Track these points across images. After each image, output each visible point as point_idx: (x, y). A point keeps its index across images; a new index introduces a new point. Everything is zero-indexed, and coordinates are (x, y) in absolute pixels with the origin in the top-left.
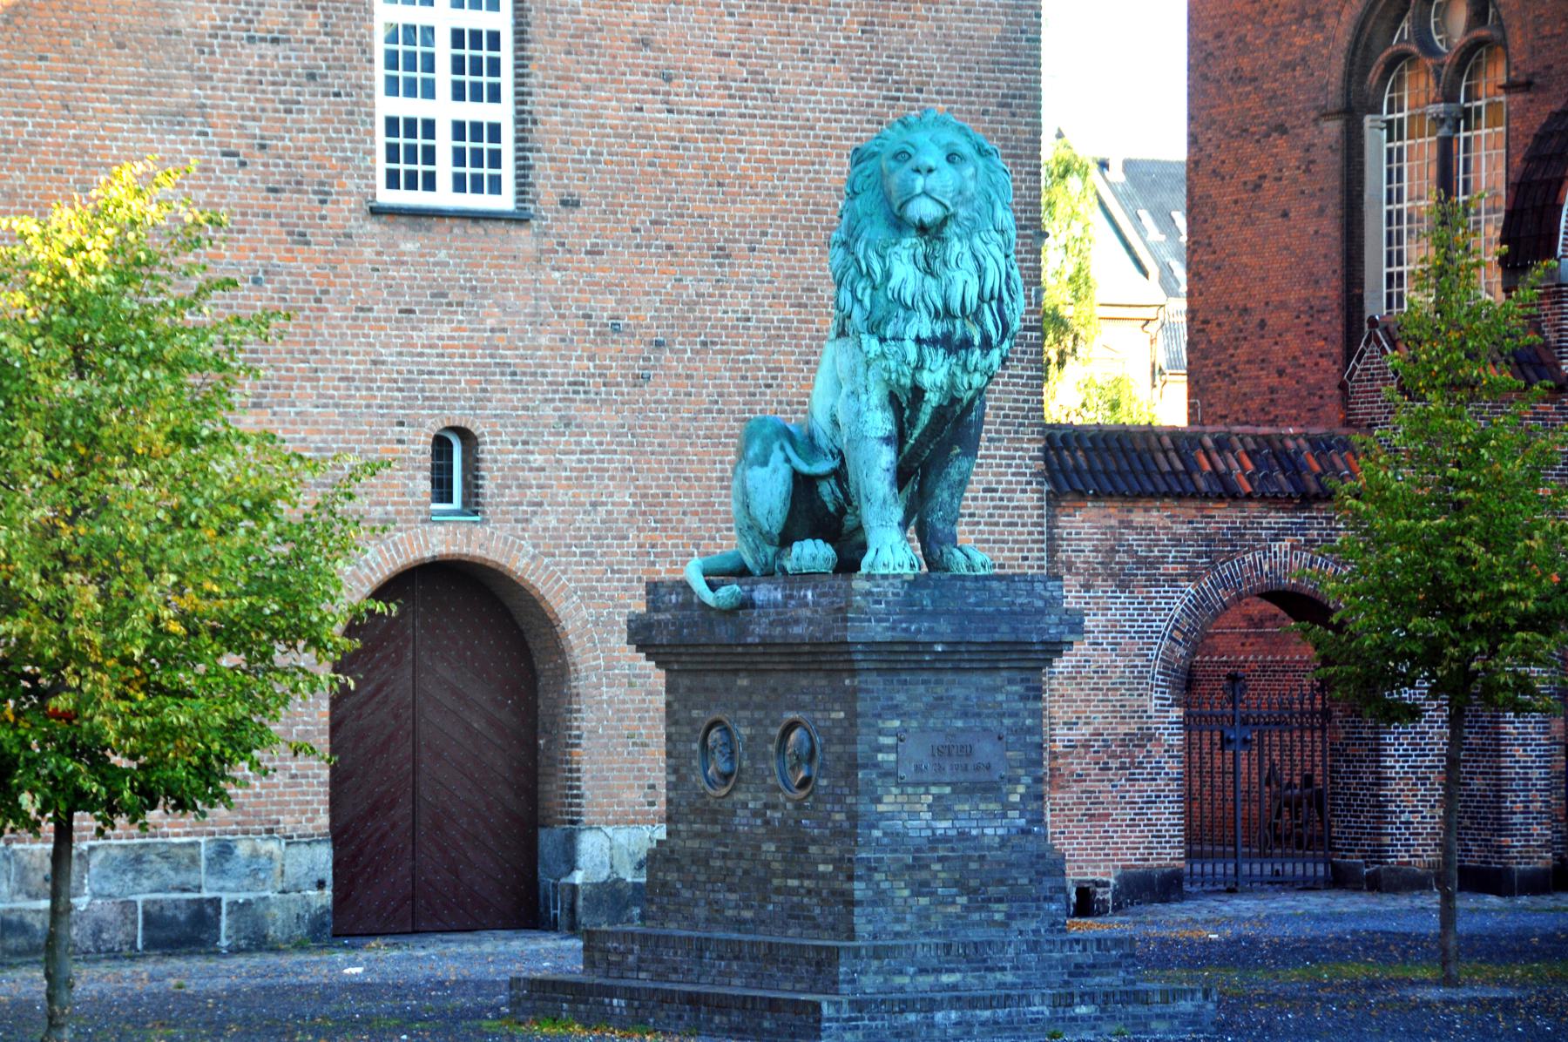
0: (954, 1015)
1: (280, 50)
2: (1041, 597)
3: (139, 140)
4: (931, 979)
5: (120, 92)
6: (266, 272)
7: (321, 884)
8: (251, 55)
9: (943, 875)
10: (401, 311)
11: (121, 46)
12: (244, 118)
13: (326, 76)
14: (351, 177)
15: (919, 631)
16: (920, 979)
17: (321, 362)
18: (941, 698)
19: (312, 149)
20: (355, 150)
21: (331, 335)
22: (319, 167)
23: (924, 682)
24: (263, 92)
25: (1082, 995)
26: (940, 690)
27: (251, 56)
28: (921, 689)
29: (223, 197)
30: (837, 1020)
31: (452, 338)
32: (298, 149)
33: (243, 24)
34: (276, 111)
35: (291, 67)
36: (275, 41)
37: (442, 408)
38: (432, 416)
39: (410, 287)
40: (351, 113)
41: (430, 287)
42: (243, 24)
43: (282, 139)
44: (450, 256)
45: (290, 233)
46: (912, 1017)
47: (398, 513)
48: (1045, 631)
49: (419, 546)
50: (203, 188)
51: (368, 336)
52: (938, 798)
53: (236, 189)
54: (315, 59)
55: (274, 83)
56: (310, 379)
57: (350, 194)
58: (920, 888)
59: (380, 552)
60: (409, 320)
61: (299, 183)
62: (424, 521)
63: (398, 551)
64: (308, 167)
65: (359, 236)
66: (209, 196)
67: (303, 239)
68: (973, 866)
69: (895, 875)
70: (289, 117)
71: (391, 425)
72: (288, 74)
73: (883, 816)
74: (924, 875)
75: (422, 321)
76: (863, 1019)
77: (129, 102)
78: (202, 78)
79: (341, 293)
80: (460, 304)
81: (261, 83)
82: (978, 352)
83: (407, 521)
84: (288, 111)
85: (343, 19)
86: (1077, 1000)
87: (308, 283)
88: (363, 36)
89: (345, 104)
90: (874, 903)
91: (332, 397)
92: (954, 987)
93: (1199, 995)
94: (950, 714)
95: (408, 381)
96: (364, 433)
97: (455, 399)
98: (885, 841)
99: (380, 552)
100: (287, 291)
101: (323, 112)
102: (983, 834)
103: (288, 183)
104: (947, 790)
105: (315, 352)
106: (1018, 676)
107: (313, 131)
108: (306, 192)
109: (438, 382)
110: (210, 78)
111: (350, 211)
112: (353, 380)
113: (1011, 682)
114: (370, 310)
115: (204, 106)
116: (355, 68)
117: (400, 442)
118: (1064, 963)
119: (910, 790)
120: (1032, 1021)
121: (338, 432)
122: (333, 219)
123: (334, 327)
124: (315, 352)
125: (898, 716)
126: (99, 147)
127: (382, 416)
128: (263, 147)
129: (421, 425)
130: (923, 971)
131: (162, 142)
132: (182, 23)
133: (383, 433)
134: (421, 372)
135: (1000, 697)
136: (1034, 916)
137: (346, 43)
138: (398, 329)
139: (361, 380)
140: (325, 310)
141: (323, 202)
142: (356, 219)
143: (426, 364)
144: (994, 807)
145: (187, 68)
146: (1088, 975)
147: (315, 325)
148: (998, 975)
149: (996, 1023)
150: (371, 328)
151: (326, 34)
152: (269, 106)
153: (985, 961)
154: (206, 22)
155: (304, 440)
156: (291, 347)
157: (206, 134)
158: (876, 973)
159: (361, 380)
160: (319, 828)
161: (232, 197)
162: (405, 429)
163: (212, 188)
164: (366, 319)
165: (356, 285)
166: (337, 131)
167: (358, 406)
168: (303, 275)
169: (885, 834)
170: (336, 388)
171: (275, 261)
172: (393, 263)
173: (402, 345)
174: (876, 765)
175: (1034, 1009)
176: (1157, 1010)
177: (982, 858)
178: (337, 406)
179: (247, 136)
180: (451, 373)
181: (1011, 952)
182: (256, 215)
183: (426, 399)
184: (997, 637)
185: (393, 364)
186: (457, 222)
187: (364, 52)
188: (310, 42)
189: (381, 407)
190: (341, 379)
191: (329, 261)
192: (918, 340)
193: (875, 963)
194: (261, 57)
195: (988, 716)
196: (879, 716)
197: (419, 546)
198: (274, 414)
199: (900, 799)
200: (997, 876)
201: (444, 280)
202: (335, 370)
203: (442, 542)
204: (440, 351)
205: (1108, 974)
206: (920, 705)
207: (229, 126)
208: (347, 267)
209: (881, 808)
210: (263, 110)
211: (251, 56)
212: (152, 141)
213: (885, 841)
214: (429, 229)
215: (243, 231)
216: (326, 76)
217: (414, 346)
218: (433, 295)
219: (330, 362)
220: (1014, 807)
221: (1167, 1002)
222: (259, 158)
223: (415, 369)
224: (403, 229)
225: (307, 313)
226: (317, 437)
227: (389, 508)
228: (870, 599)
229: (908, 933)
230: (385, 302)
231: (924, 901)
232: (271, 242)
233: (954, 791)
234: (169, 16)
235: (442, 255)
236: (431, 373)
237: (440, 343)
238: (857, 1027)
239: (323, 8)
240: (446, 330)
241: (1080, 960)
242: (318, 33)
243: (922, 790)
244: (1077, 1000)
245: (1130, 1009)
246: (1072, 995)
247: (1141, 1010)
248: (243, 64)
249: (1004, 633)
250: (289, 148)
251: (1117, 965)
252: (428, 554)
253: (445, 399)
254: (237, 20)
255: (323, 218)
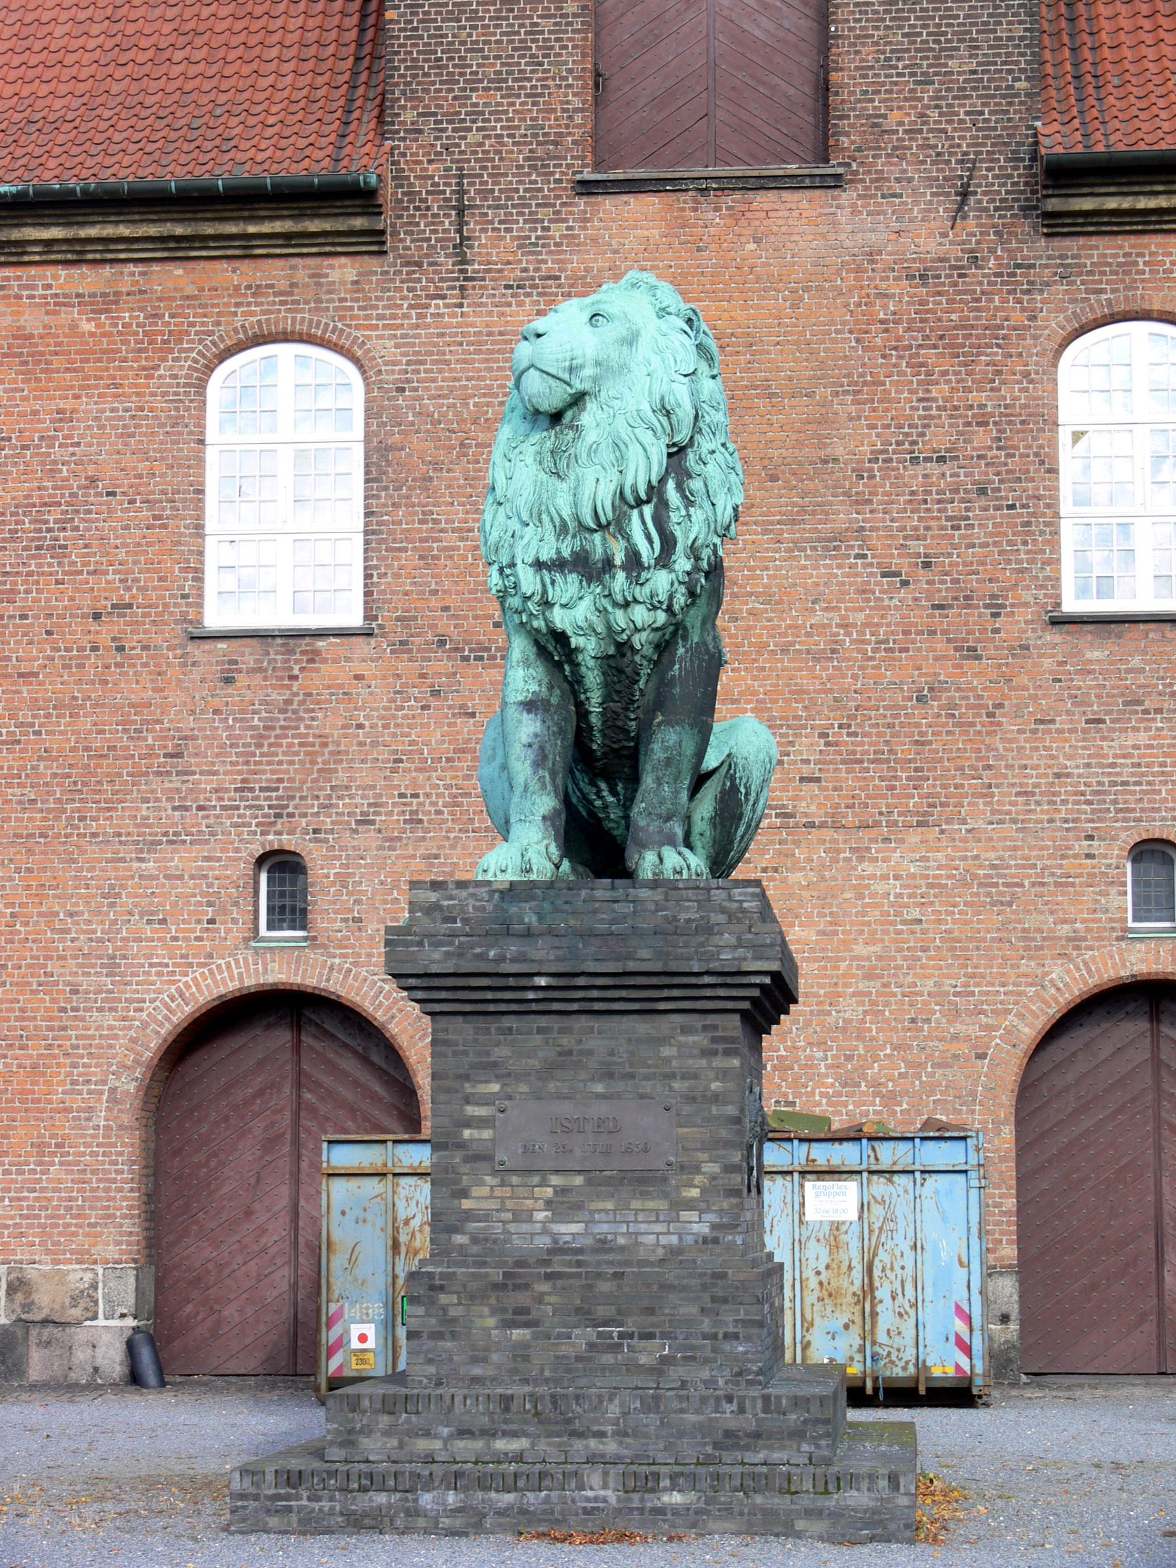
0: (451, 1498)
1: (947, 468)
2: (723, 910)
3: (791, 568)
4: (479, 1444)
5: (772, 523)
6: (931, 689)
7: (1005, 1319)
8: (914, 477)
9: (553, 1299)
10: (1088, 722)
11: (774, 478)
12: (905, 538)
13: (999, 490)
14: (1028, 588)
15: (501, 959)
16: (461, 1444)
17: (996, 776)
18: (570, 1053)
19: (983, 564)
20: (1031, 561)
21: (1005, 749)
22: (990, 580)
23: (540, 1031)
24: (928, 510)
25: (673, 1477)
26: (566, 1041)
27: (915, 476)
28: (538, 1039)
29: (882, 617)
30: (256, 1498)
31: (1151, 746)
32: (965, 564)
33: (907, 446)
34: (942, 528)
35: (958, 484)
36: (941, 459)
37: (1140, 820)
38: (1127, 829)
39: (1098, 696)
40: (1028, 524)
41: (1123, 695)
42: (907, 446)
43: (950, 555)
44: (1146, 662)
45: (956, 649)
46: (381, 1498)
47: (1089, 930)
48: (714, 956)
49: (1114, 965)
50: (862, 610)
51: (1050, 749)
52: (561, 1191)
53: (896, 608)
54: (986, 474)
55: (939, 502)
56: (984, 796)
57: (1026, 605)
58: (519, 1317)
59: (1068, 972)
60: (1098, 731)
61: (967, 598)
62: (1118, 939)
63: (1089, 971)
64: (978, 581)
65: (1035, 647)
66: (867, 616)
67: (973, 654)
68: (605, 1286)
69: (472, 1298)
70: (957, 533)
71: (1078, 839)
72: (956, 491)
73: (469, 1215)
74: (522, 1299)
75: (1114, 730)
76: (298, 1498)
77: (781, 532)
78: (861, 502)
79: (1017, 706)
80: (1159, 711)
81: (925, 502)
82: (621, 576)
83: (1100, 939)
84: (956, 528)
85: (1018, 432)
86: (665, 1483)
87: (980, 697)
88: (1041, 447)
89: (1020, 515)
90: (437, 1336)
91: (1008, 813)
92: (519, 1458)
93: (883, 1483)
94: (583, 1075)
95: (1098, 793)
96: (1046, 848)
97: (1153, 810)
98: (475, 1249)
99: (1068, 972)
100: (956, 707)
101: (995, 525)
102: (637, 1244)
103: (956, 598)
104: (579, 1180)
105: (989, 767)
106: (696, 1021)
107: (985, 545)
108: (978, 607)
109: (1134, 793)
110: (870, 502)
111: (1026, 622)
112: (1033, 794)
113: (685, 1030)
114: (1052, 721)
115: (863, 529)
116: (1032, 480)
117: (1089, 856)
118: (704, 1429)
119: (515, 1180)
120: (586, 1511)
121: (1015, 849)
122: (1007, 632)
123: (1010, 741)
124: (989, 767)
125: (498, 1077)
126: (749, 578)
127: (1068, 830)
128: (927, 565)
129: (1113, 839)
130: (464, 1433)
131: (816, 568)
132: (839, 451)
133: (1068, 848)
134: (1115, 784)
135: (666, 1051)
136: (706, 1361)
137: (1021, 456)
138: (1084, 740)
139: (1042, 794)
140: (999, 724)
141: (995, 615)
142: (1034, 630)
143: (1119, 774)
144: (662, 1204)
145: (844, 494)
146: (747, 1448)
147: (987, 740)
148: (593, 1443)
149: (523, 1512)
150: (1053, 740)
151: (999, 448)
152: (933, 523)
153: (569, 1421)
154: (866, 448)
155: (977, 857)
156: (960, 763)
157: (864, 556)
158: (387, 1433)
159: (1042, 794)
160: (1002, 1258)
161: (894, 616)
162: (1095, 843)
163: (871, 608)
164: (1049, 732)
165: (1034, 698)
166: (1010, 543)
167: (1037, 822)
168: (975, 689)
169: (475, 1240)
170: (1011, 804)
171: (942, 678)
172: (1077, 672)
173: (1090, 756)
174: (461, 1145)
175: (590, 1493)
176: (805, 1501)
177: (618, 1276)
178: (1014, 821)
179: (910, 555)
180: (1149, 783)
181: (614, 1410)
182: (918, 633)
183: (1118, 811)
184: (632, 966)
185: (1079, 776)
186: (1153, 626)
187: (1042, 463)
188: (980, 457)
189: (1066, 821)
190: (1018, 794)
191: (1003, 674)
192: (539, 565)
193: (385, 1420)
194: (925, 476)
195: (647, 1078)
196: (467, 1078)
197: (1114, 965)
198: (942, 832)
199: (498, 1192)
200: (646, 1303)
201: (1139, 687)
202: (1013, 785)
203: (1142, 961)
204: (1136, 760)
205: (783, 1448)
206: (534, 1063)
207: (890, 546)
208: (1025, 680)
209: (466, 1204)
210: (927, 528)
211: (915, 476)
212: (805, 567)
213: (475, 1249)
214: (1119, 636)
215: (907, 650)
216: (999, 490)
217: (1105, 756)
218: (1125, 704)
219: (1005, 777)
220: (690, 1205)
221: (827, 1492)
222: (923, 575)
223: (1106, 780)
224: (1089, 637)
225: (978, 728)
226: (992, 855)
227: (1078, 925)
228: (437, 915)
229: (494, 1379)
230: (1068, 713)
231: (517, 1334)
232: (936, 659)
233: (589, 1182)
234: (825, 445)
235: (1136, 661)
236: (1124, 783)
237: (1136, 752)
238: (289, 1509)
239: (995, 423)
240: (1143, 738)
241: (733, 1425)
242: (990, 448)
243: (536, 1179)
244: (665, 1483)
245: (759, 1499)
246: (657, 1477)
247: (779, 1502)
248: (905, 485)
249: (645, 958)
250: (957, 564)
251: (798, 1434)
252: (1124, 973)
253: (1142, 810)
254: (898, 443)
255: (996, 631)
